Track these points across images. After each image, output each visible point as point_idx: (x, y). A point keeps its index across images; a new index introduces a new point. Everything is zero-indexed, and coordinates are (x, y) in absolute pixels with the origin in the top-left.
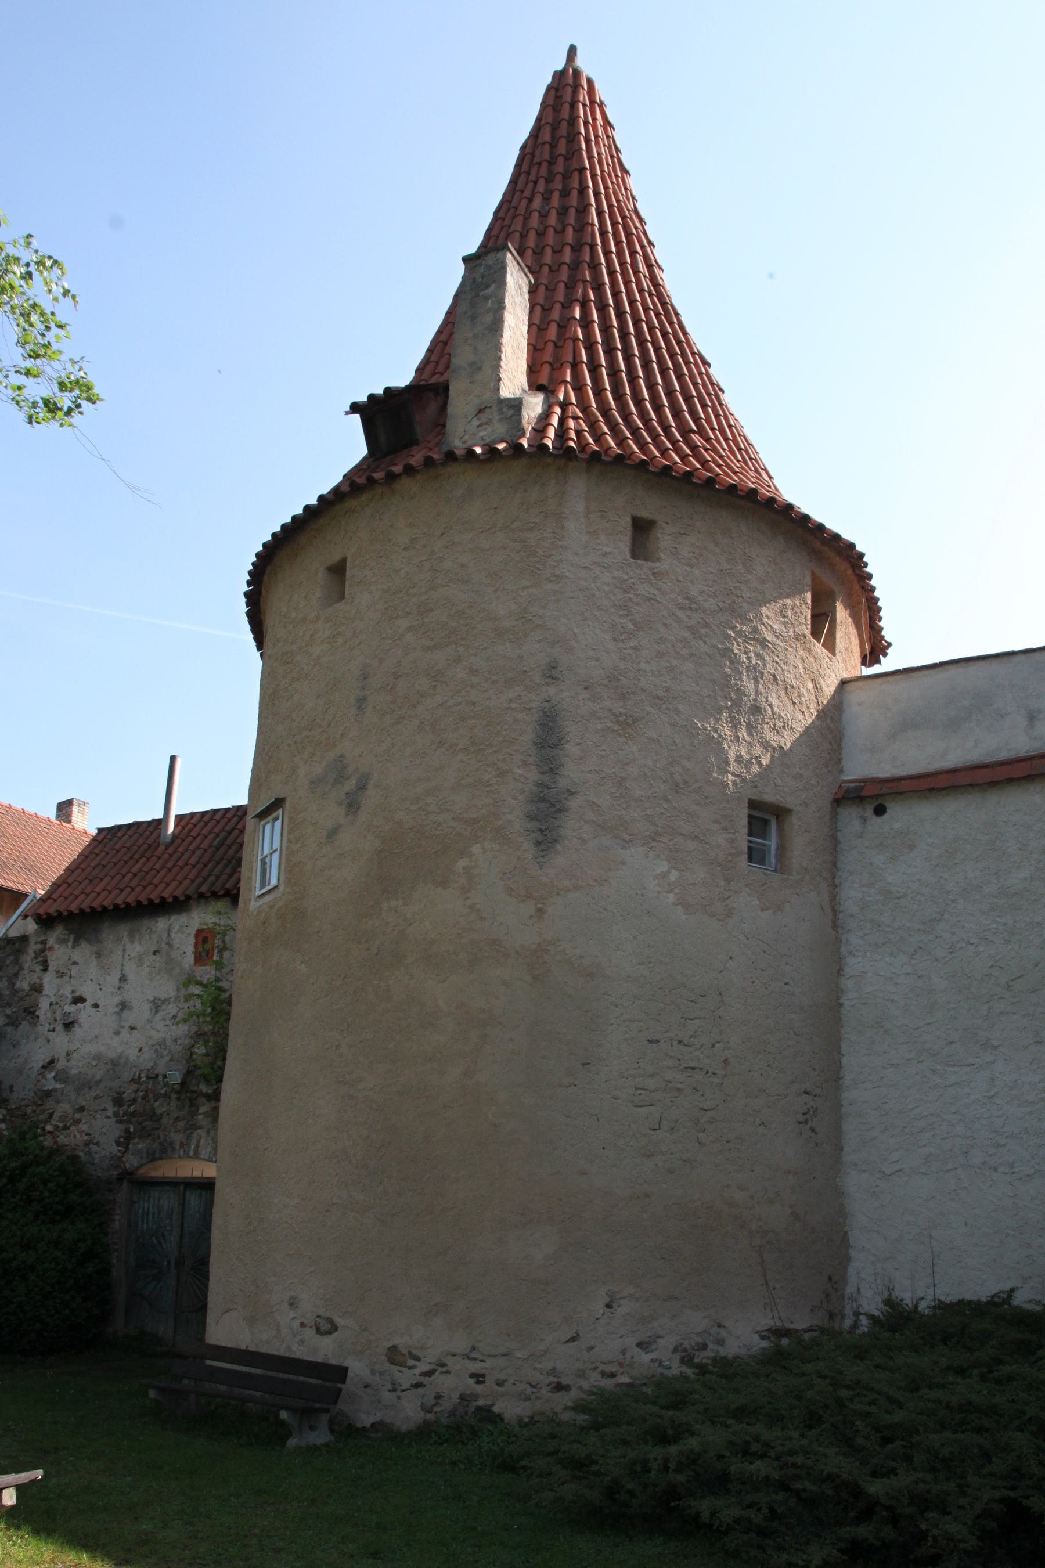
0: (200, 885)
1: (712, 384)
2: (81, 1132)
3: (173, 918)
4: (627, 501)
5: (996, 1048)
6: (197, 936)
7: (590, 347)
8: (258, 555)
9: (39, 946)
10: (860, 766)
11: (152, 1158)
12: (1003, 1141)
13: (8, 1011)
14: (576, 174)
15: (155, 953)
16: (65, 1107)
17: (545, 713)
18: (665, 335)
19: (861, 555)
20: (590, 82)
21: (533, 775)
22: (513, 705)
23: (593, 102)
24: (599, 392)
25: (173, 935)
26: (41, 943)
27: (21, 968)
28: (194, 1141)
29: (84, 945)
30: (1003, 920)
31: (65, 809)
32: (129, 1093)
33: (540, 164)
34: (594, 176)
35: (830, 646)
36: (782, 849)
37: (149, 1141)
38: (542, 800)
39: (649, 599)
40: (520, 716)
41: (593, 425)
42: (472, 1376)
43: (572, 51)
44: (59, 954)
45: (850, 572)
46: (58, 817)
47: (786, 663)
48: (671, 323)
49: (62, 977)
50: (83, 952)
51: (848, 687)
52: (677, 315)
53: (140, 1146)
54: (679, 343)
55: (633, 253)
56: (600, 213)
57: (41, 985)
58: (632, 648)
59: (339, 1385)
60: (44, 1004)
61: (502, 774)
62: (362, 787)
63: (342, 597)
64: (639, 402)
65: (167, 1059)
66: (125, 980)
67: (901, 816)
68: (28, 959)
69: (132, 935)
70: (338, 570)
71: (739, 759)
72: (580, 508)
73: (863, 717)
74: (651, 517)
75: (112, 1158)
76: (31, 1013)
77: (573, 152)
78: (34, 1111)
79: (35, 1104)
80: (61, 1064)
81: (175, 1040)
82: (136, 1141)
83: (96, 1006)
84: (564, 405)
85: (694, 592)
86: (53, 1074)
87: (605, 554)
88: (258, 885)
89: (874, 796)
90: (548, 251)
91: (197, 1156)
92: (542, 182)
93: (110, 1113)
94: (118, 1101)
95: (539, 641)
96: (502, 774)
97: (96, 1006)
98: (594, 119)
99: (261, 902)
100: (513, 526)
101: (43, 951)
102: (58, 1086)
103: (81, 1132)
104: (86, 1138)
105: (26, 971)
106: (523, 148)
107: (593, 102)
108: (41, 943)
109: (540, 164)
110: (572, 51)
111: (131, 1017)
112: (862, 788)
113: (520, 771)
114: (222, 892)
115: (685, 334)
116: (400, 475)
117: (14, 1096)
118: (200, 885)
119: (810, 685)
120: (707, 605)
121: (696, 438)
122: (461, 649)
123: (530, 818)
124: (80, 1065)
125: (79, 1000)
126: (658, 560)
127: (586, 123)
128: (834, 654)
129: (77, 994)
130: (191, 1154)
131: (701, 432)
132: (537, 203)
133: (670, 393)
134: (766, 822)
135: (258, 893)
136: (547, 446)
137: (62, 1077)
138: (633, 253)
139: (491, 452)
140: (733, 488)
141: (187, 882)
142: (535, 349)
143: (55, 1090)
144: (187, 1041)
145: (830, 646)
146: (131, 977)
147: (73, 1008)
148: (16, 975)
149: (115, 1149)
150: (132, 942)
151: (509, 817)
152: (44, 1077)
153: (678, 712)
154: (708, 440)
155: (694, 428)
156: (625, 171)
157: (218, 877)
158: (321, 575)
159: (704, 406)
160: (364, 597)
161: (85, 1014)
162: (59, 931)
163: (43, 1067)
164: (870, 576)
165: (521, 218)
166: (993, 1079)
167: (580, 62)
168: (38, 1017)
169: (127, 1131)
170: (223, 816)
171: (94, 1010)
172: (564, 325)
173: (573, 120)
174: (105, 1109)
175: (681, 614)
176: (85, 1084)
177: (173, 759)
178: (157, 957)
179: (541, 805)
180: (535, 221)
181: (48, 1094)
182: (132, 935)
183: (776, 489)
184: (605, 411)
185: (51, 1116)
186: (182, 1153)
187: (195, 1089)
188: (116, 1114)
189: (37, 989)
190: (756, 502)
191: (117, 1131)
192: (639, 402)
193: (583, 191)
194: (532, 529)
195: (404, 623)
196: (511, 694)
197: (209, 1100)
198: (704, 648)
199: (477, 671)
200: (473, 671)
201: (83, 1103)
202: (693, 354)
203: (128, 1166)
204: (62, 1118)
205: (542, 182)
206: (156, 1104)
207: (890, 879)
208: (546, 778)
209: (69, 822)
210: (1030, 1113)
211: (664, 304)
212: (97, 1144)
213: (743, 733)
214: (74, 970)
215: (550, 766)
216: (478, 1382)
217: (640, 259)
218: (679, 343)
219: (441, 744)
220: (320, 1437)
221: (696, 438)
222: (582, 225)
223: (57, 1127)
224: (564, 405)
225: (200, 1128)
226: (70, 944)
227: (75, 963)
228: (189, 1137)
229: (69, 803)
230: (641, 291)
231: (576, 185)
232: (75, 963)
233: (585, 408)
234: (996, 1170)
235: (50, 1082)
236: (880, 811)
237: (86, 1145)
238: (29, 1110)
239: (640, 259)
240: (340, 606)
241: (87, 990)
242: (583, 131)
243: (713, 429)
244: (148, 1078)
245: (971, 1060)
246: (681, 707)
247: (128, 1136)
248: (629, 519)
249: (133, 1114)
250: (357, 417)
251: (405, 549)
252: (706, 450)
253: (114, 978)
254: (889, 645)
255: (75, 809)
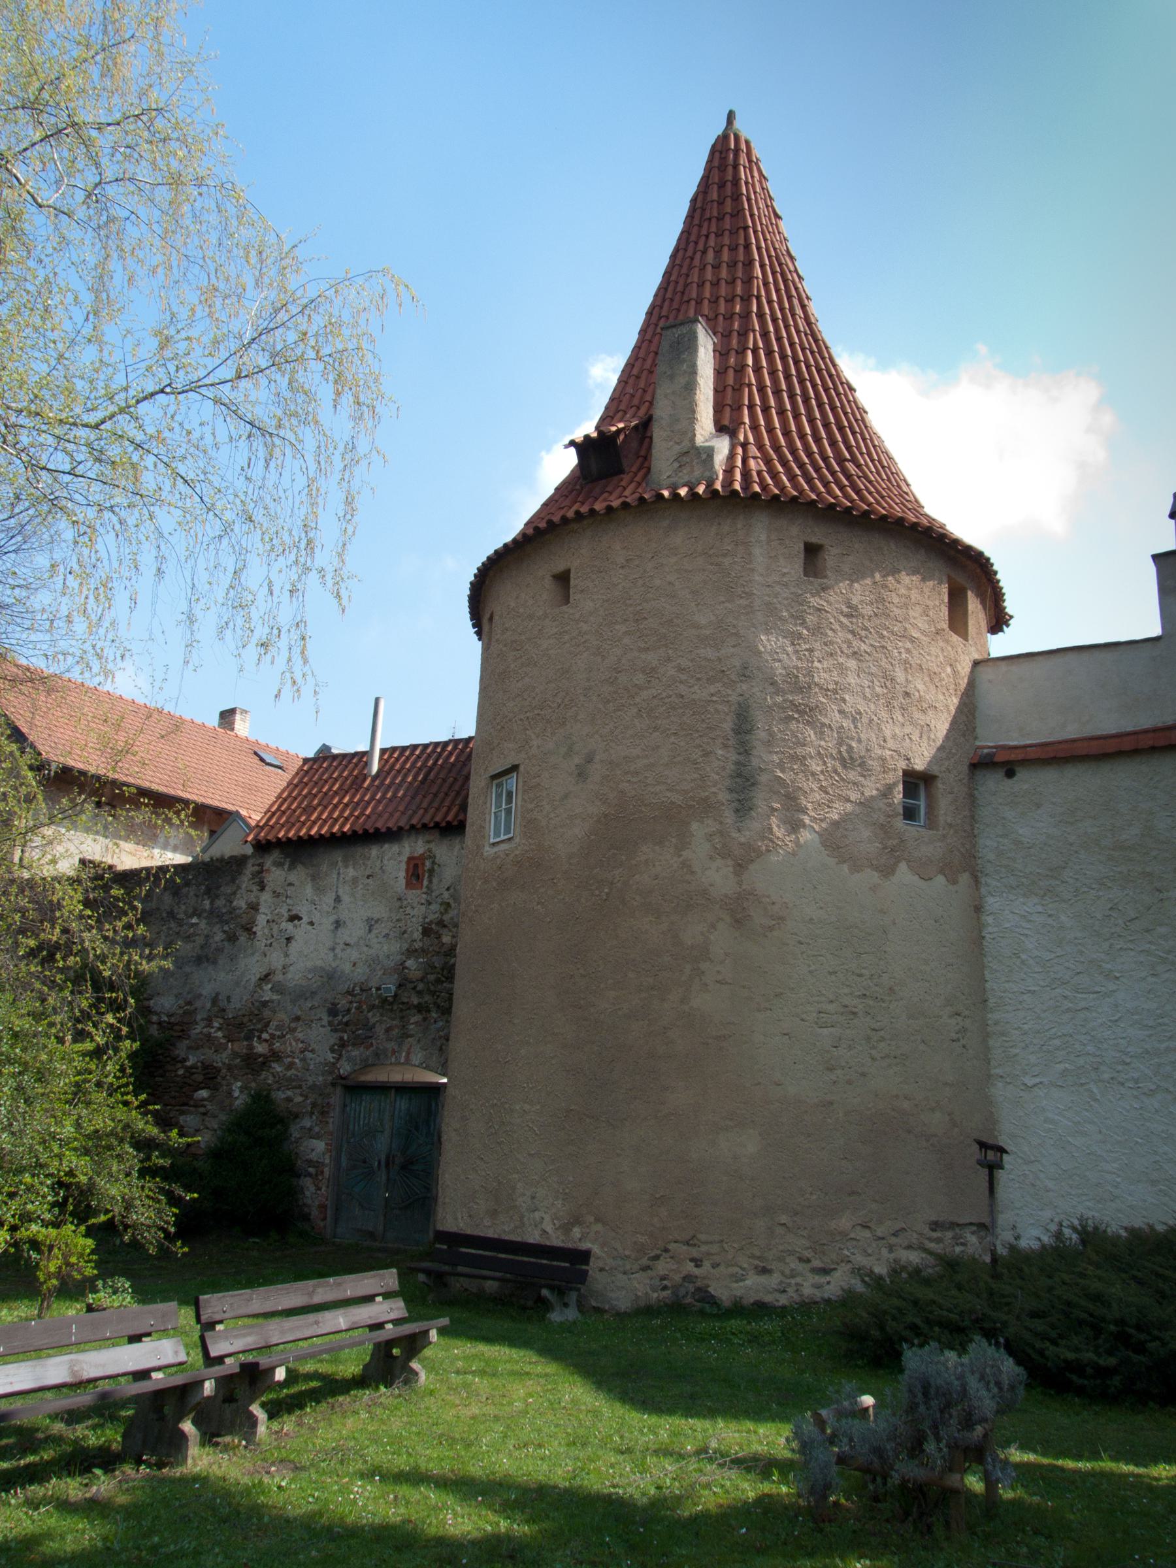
0: (411, 818)
1: (858, 408)
2: (297, 1040)
3: (386, 846)
4: (797, 532)
5: (1117, 978)
6: (408, 862)
7: (762, 389)
8: (488, 558)
9: (257, 868)
10: (990, 738)
11: (366, 1066)
12: (1128, 1060)
13: (226, 928)
14: (741, 232)
15: (368, 877)
16: (282, 1016)
17: (739, 704)
18: (819, 371)
19: (988, 559)
20: (747, 143)
21: (734, 757)
22: (714, 699)
23: (750, 161)
24: (771, 430)
25: (386, 862)
26: (259, 865)
27: (239, 887)
28: (405, 1048)
29: (300, 867)
30: (1119, 869)
31: (227, 717)
32: (343, 1003)
33: (710, 219)
34: (755, 232)
35: (964, 635)
36: (931, 808)
37: (362, 1049)
38: (740, 775)
39: (819, 610)
40: (720, 707)
41: (768, 462)
42: (692, 1260)
43: (731, 116)
44: (276, 875)
45: (978, 570)
46: (221, 725)
47: (929, 654)
48: (823, 358)
49: (278, 897)
50: (299, 875)
51: (980, 668)
52: (827, 348)
53: (353, 1054)
54: (831, 376)
55: (790, 297)
56: (762, 266)
57: (258, 904)
58: (807, 650)
59: (584, 1267)
60: (261, 919)
61: (707, 754)
62: (589, 759)
63: (566, 600)
64: (802, 437)
65: (380, 973)
66: (340, 901)
67: (1026, 780)
68: (245, 880)
69: (346, 861)
70: (563, 579)
71: (894, 736)
72: (763, 537)
73: (996, 696)
74: (819, 542)
75: (326, 1064)
76: (249, 929)
77: (738, 213)
78: (250, 1021)
79: (252, 1013)
80: (279, 977)
81: (388, 956)
82: (350, 1048)
83: (312, 923)
84: (744, 446)
85: (855, 601)
86: (270, 986)
87: (784, 575)
88: (492, 833)
89: (1003, 764)
90: (722, 302)
91: (408, 1062)
92: (712, 236)
93: (325, 1022)
94: (333, 1011)
95: (734, 646)
96: (707, 754)
97: (312, 923)
98: (752, 177)
99: (496, 849)
100: (711, 553)
101: (261, 872)
102: (275, 997)
103: (297, 1040)
104: (301, 1045)
105: (243, 891)
106: (694, 201)
107: (750, 161)
108: (259, 865)
109: (710, 219)
110: (731, 116)
111: (344, 935)
112: (994, 754)
113: (720, 752)
114: (432, 825)
115: (834, 365)
116: (617, 509)
117: (232, 1006)
118: (411, 818)
119: (949, 670)
120: (864, 612)
121: (850, 466)
122: (670, 652)
123: (731, 790)
124: (297, 977)
125: (294, 918)
126: (825, 577)
127: (747, 183)
128: (966, 640)
129: (294, 912)
130: (402, 1060)
131: (854, 460)
132: (710, 255)
133: (826, 425)
134: (916, 786)
135: (492, 841)
136: (736, 491)
137: (278, 989)
138: (790, 297)
139: (693, 495)
140: (883, 518)
141: (398, 814)
142: (719, 391)
143: (272, 1001)
144: (399, 957)
145: (964, 635)
146: (346, 899)
147: (290, 926)
148: (234, 893)
149: (330, 1057)
150: (346, 867)
151: (714, 790)
152: (261, 989)
153: (844, 700)
154: (859, 466)
155: (848, 457)
156: (777, 216)
157: (426, 810)
158: (548, 582)
159: (854, 433)
160: (588, 599)
161: (300, 932)
162: (276, 855)
163: (260, 979)
164: (996, 573)
165: (697, 270)
166: (1116, 1006)
167: (738, 124)
168: (255, 933)
169: (341, 1039)
170: (423, 752)
171: (310, 927)
172: (741, 369)
173: (736, 181)
174: (320, 1019)
175: (843, 619)
176: (303, 994)
177: (377, 700)
178: (370, 881)
179: (738, 780)
180: (709, 273)
181: (265, 1004)
182: (346, 861)
183: (916, 501)
184: (777, 449)
185: (267, 1025)
186: (393, 1060)
187: (405, 1000)
188: (330, 1023)
189: (254, 907)
190: (903, 526)
191: (333, 1039)
192: (802, 437)
193: (747, 246)
194: (725, 555)
195: (622, 628)
196: (712, 689)
197: (419, 1011)
198: (863, 647)
199: (684, 669)
200: (680, 669)
201: (299, 1013)
202: (842, 383)
203: (342, 1071)
204: (278, 1028)
205: (712, 236)
206: (370, 1014)
207: (1021, 832)
208: (741, 758)
209: (233, 729)
210: (1150, 1036)
211: (816, 341)
212: (312, 1051)
213: (898, 715)
214: (290, 891)
215: (745, 750)
216: (697, 1266)
217: (796, 301)
218: (831, 376)
219: (656, 729)
220: (571, 1314)
221: (850, 466)
222: (749, 280)
223: (273, 1036)
224: (744, 446)
225: (411, 1036)
226: (286, 867)
227: (290, 884)
228: (400, 1045)
229: (232, 711)
230: (798, 332)
231: (742, 241)
232: (290, 884)
233: (761, 447)
234: (1123, 1084)
235: (267, 994)
236: (1010, 774)
237: (302, 1052)
238: (245, 1020)
239: (796, 301)
240: (565, 608)
241: (303, 910)
242: (745, 192)
243: (862, 454)
244: (362, 990)
245: (1097, 989)
246: (847, 697)
247: (343, 1044)
248: (802, 546)
249: (347, 1024)
250: (573, 450)
251: (622, 567)
252: (859, 477)
253: (329, 899)
254: (1011, 617)
255: (238, 717)
